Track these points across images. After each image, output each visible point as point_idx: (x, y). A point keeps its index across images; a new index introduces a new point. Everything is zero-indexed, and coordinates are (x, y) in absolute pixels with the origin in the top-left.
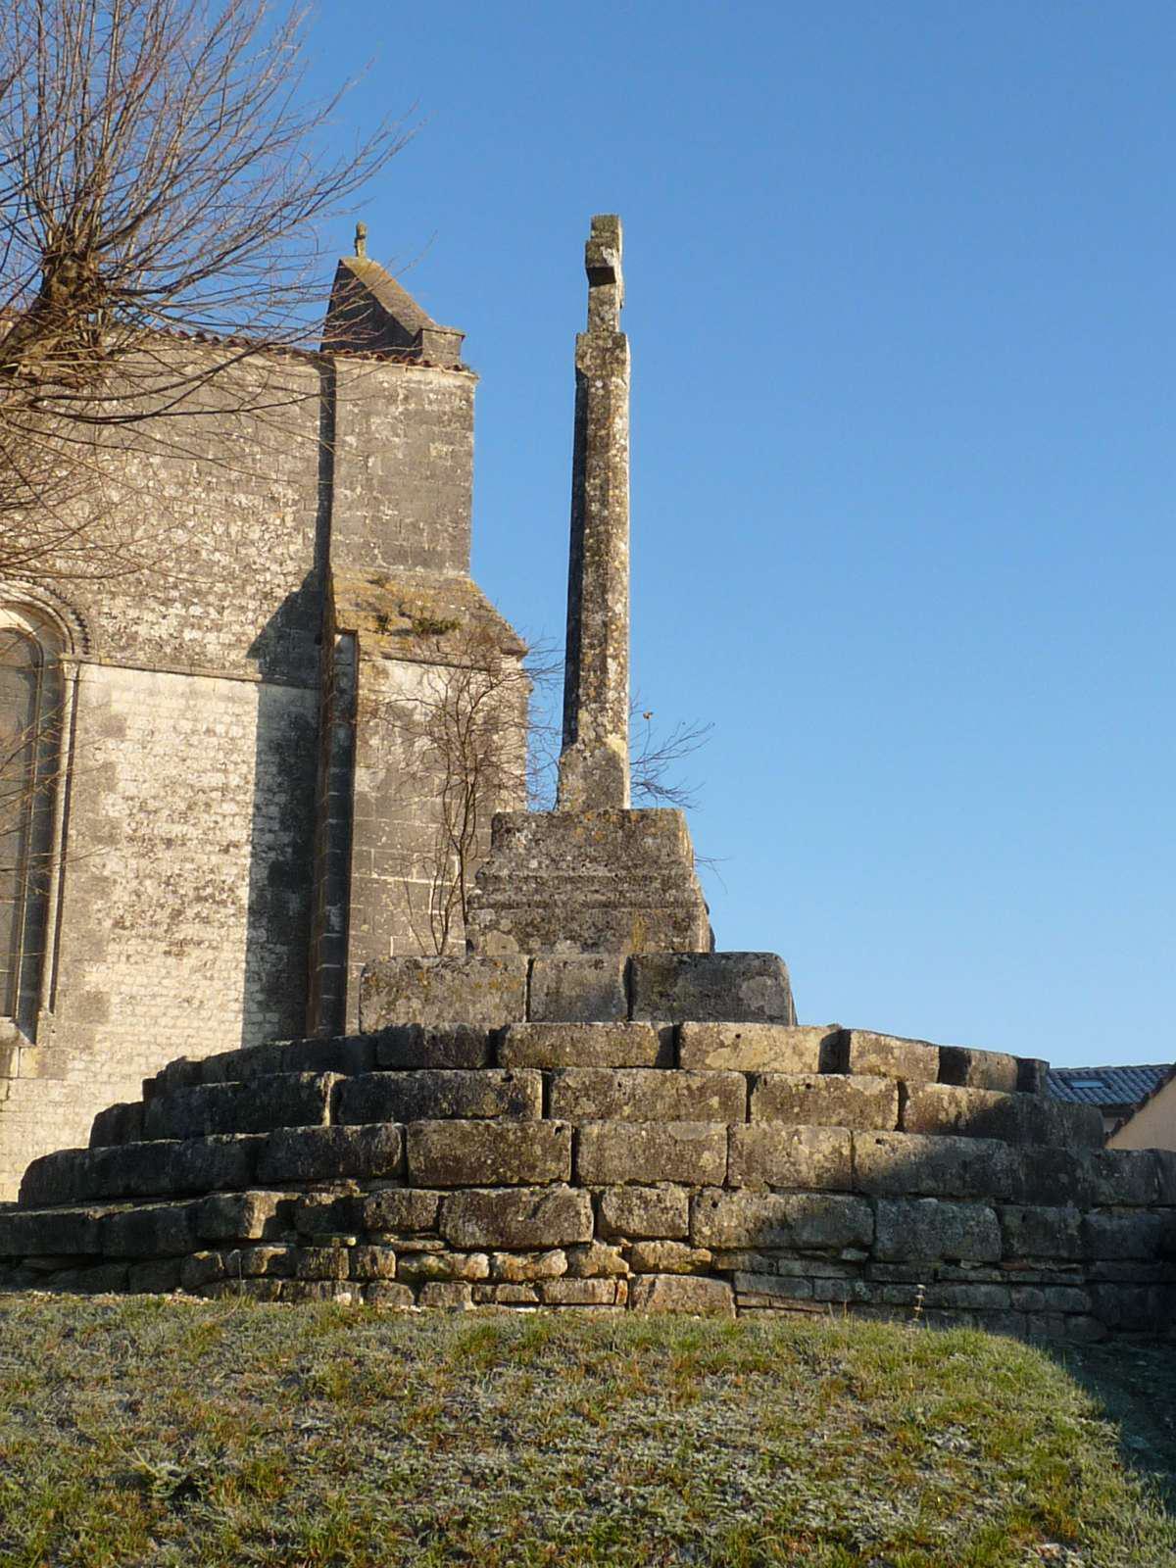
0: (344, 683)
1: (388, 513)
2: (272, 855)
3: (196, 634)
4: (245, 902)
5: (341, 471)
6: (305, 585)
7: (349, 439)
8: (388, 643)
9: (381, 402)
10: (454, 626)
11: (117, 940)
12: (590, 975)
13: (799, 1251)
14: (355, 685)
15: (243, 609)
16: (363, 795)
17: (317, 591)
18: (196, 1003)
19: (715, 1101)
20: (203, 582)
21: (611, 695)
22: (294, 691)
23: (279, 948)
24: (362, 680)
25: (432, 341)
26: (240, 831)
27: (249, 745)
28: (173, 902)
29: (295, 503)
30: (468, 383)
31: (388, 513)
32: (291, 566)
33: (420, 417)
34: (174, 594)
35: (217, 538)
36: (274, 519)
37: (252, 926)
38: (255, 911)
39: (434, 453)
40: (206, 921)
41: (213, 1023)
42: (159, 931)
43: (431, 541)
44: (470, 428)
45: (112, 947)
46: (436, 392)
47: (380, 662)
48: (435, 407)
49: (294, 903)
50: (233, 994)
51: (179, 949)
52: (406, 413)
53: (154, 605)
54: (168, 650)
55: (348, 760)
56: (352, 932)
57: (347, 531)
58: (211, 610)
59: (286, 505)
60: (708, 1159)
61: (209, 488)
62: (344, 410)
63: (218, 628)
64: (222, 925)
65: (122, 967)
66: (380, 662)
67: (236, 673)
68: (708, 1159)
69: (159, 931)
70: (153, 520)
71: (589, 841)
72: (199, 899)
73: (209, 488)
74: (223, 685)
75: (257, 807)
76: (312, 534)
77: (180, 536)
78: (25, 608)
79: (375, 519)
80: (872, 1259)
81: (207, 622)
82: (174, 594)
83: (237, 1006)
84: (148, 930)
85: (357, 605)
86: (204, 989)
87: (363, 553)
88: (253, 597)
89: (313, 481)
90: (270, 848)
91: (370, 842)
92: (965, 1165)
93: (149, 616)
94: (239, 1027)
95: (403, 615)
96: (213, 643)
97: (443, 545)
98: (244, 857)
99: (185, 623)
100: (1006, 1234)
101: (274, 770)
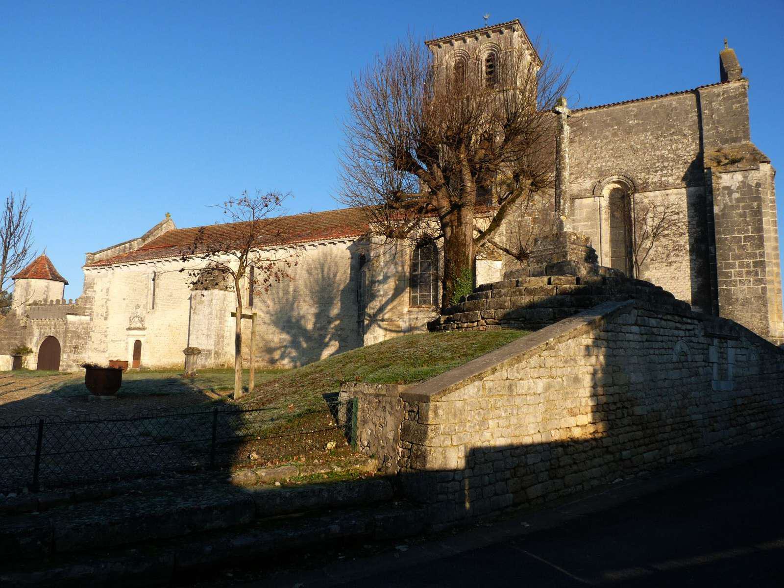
0: (709, 183)
1: (721, 129)
2: (695, 235)
3: (666, 178)
4: (688, 249)
5: (704, 121)
6: (697, 157)
7: (706, 111)
8: (720, 168)
9: (715, 98)
10: (742, 159)
11: (652, 264)
12: (539, 269)
13: (514, 319)
14: (712, 183)
15: (679, 168)
16: (717, 214)
17: (700, 156)
18: (676, 278)
19: (518, 293)
20: (666, 164)
21: (561, 207)
22: (697, 188)
23: (700, 260)
24: (713, 181)
25: (731, 74)
26: (684, 229)
27: (684, 206)
28: (667, 252)
29: (691, 134)
30: (744, 83)
31: (721, 129)
32: (692, 153)
33: (729, 98)
34: (658, 169)
35: (669, 150)
36: (685, 141)
37: (691, 255)
38: (691, 251)
39: (734, 108)
40: (677, 256)
41: (682, 283)
42: (664, 260)
43: (736, 134)
44: (746, 97)
45: (651, 266)
46: (733, 89)
47: (719, 175)
48: (733, 94)
49: (703, 247)
50: (687, 275)
51: (670, 264)
52: (724, 99)
53: (652, 173)
54: (658, 184)
55: (712, 206)
56: (717, 253)
57: (708, 138)
58: (669, 171)
59: (689, 135)
60: (506, 304)
61: (665, 137)
62: (703, 103)
63: (672, 175)
64: (682, 256)
65: (654, 271)
66: (719, 175)
67: (678, 186)
68: (506, 304)
69: (664, 260)
70: (650, 150)
71: (551, 241)
72: (674, 250)
73: (665, 137)
74: (675, 191)
75: (689, 222)
76: (698, 142)
77: (658, 153)
78: (618, 182)
79: (717, 132)
80: (526, 320)
81: (668, 174)
82: (658, 169)
83: (689, 278)
84: (661, 260)
85: (711, 159)
86: (678, 274)
87: (714, 144)
88: (681, 164)
89: (696, 127)
90: (694, 233)
91: (720, 227)
92: (558, 301)
93: (652, 177)
94: (690, 283)
95: (726, 159)
96: (671, 180)
97: (741, 134)
98: (686, 237)
99: (662, 176)
100: (554, 313)
101: (693, 211)
